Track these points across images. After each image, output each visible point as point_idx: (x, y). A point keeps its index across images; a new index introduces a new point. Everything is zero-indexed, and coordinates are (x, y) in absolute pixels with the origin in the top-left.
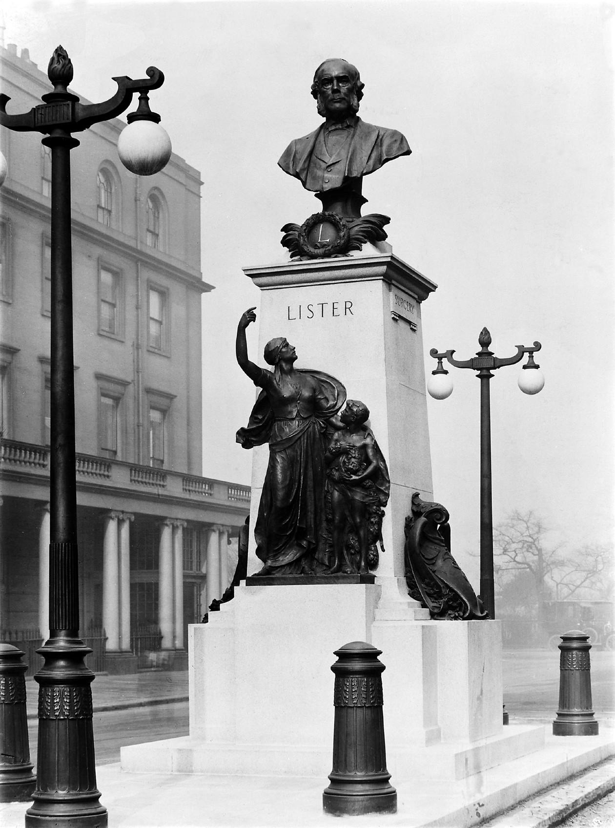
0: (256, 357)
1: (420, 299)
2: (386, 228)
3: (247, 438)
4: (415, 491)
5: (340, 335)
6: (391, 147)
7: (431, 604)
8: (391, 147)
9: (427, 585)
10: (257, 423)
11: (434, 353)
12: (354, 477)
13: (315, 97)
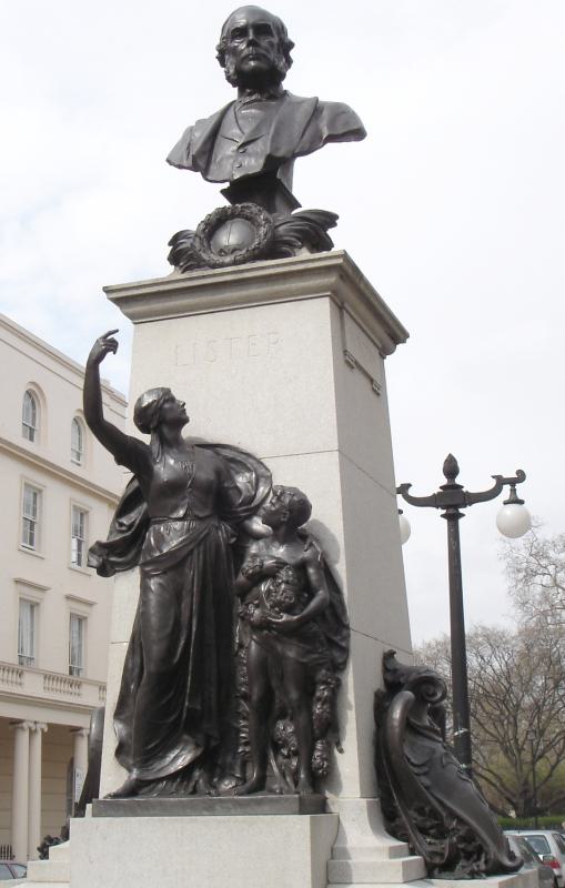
1: (385, 351)
2: (330, 232)
3: (110, 559)
4: (387, 649)
5: (256, 387)
9: (420, 811)
10: (122, 532)
12: (285, 617)
13: (223, 64)
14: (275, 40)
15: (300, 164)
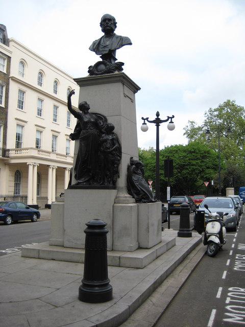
1: (135, 92)
2: (123, 67)
5: (103, 101)
6: (125, 42)
7: (136, 196)
8: (125, 42)
11: (143, 118)
14: (112, 22)
15: (118, 52)
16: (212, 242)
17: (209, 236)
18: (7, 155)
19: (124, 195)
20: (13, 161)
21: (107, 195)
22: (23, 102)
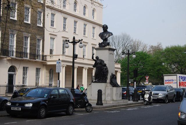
0: (95, 58)
16: (146, 100)
17: (145, 99)
18: (44, 59)
19: (109, 85)
20: (49, 63)
21: (103, 85)
22: (53, 21)
